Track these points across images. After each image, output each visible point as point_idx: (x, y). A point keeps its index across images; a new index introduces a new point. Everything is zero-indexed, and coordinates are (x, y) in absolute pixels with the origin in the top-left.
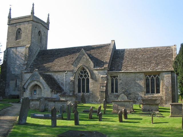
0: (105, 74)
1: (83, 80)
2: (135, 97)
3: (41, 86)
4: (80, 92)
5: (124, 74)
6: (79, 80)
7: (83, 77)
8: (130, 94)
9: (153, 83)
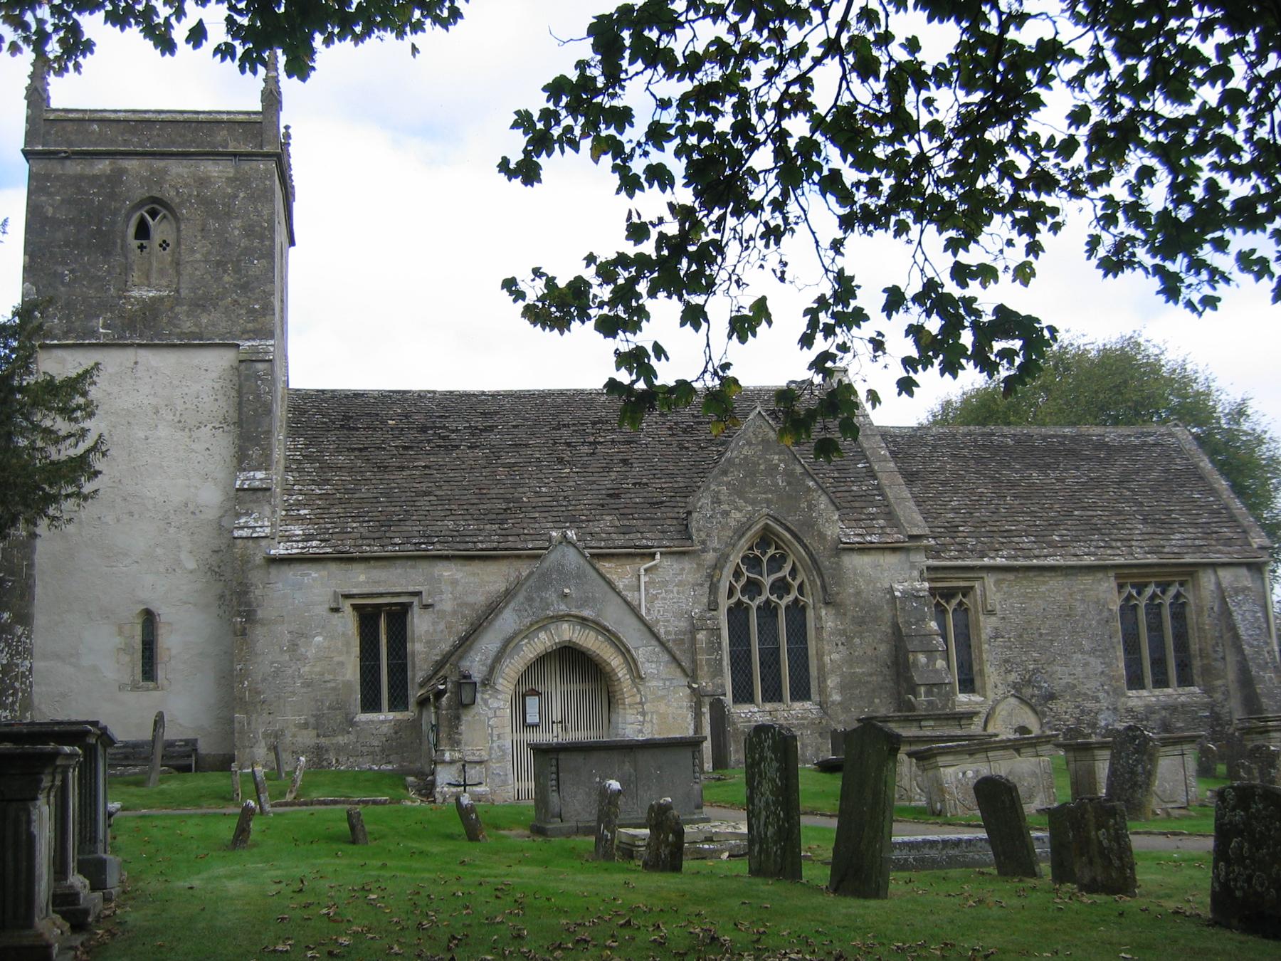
0: (916, 573)
1: (768, 611)
2: (1083, 711)
3: (615, 661)
4: (750, 699)
5: (1011, 576)
6: (738, 614)
7: (766, 594)
8: (1052, 697)
9: (1156, 627)
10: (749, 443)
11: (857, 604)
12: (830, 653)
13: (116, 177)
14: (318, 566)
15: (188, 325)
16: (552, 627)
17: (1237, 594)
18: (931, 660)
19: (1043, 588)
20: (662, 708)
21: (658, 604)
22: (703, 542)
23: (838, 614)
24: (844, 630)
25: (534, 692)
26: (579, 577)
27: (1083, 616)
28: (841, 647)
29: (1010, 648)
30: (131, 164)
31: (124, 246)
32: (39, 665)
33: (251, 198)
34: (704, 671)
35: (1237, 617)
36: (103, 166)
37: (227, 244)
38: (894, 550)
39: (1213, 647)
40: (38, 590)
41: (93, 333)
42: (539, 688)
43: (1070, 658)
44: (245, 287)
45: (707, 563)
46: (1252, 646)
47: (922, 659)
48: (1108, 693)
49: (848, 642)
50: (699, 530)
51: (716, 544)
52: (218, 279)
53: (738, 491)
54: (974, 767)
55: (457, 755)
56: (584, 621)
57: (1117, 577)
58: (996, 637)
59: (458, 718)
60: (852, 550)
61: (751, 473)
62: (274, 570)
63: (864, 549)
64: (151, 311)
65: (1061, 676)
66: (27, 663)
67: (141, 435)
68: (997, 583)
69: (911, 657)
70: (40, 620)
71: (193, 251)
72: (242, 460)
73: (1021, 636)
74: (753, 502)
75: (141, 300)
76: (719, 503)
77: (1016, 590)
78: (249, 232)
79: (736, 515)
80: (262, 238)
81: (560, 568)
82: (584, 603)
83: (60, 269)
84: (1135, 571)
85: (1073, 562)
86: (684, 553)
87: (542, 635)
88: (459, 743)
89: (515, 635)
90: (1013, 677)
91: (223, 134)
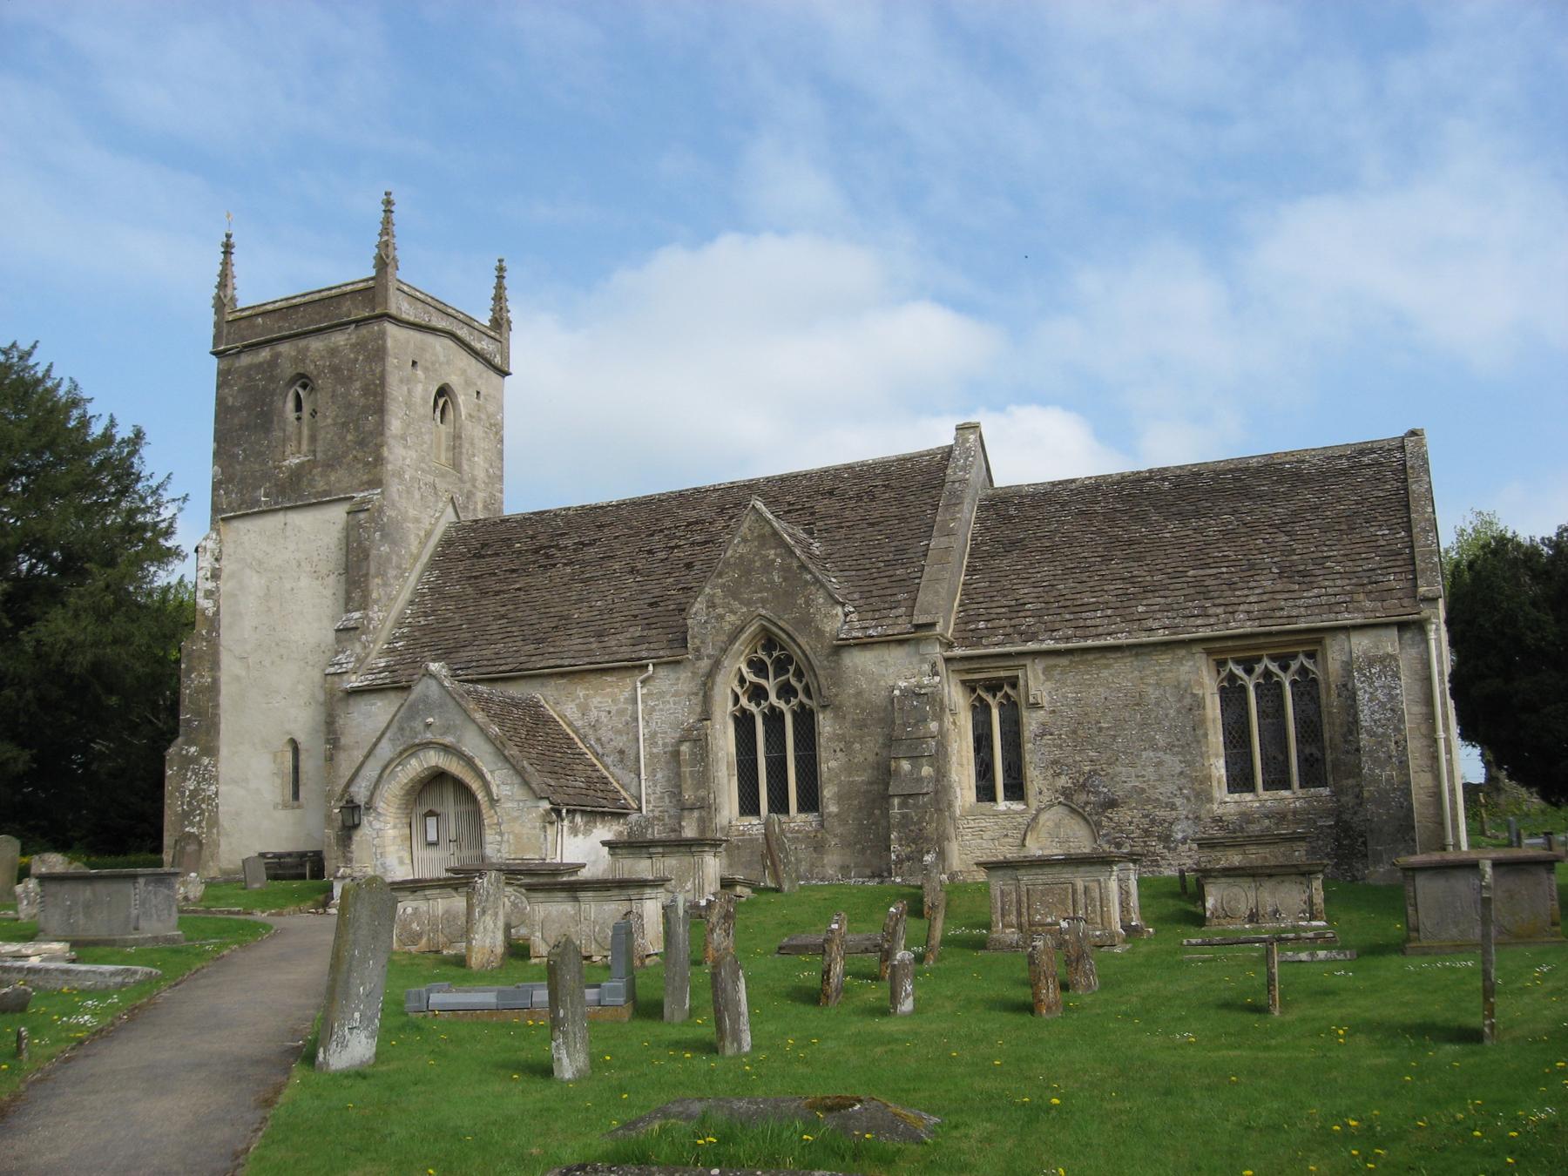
2: (1153, 822)
3: (475, 786)
5: (1064, 661)
8: (1112, 804)
10: (745, 540)
11: (857, 706)
12: (827, 761)
13: (273, 362)
14: (380, 696)
15: (321, 485)
16: (421, 754)
17: (1371, 665)
18: (916, 767)
19: (1105, 673)
20: (517, 828)
21: (656, 715)
22: (697, 650)
23: (836, 717)
24: (844, 736)
25: (431, 813)
26: (441, 706)
27: (1157, 704)
28: (839, 754)
29: (1060, 747)
30: (284, 348)
31: (283, 420)
32: (223, 789)
33: (368, 359)
34: (688, 784)
35: (1362, 697)
36: (265, 354)
37: (350, 406)
38: (901, 642)
39: (1344, 736)
40: (223, 726)
41: (257, 502)
42: (438, 810)
43: (1139, 756)
44: (362, 443)
45: (701, 671)
46: (1372, 734)
47: (906, 765)
48: (1188, 799)
49: (848, 749)
50: (694, 637)
51: (710, 651)
52: (343, 439)
53: (733, 592)
54: (415, 904)
55: (348, 871)
56: (446, 749)
57: (1209, 652)
58: (1043, 735)
59: (350, 838)
60: (849, 646)
61: (747, 572)
62: (351, 701)
63: (865, 644)
64: (297, 474)
65: (1125, 778)
66: (213, 788)
67: (288, 586)
68: (1046, 670)
69: (893, 764)
70: (224, 751)
71: (325, 417)
72: (348, 604)
73: (1074, 732)
74: (748, 603)
75: (289, 467)
76: (714, 606)
77: (1070, 678)
78: (366, 391)
79: (730, 618)
80: (375, 394)
81: (425, 699)
82: (447, 730)
83: (236, 450)
84: (1230, 643)
85: (1144, 638)
86: (678, 662)
87: (413, 762)
88: (351, 860)
89: (392, 760)
90: (1063, 781)
91: (347, 304)
